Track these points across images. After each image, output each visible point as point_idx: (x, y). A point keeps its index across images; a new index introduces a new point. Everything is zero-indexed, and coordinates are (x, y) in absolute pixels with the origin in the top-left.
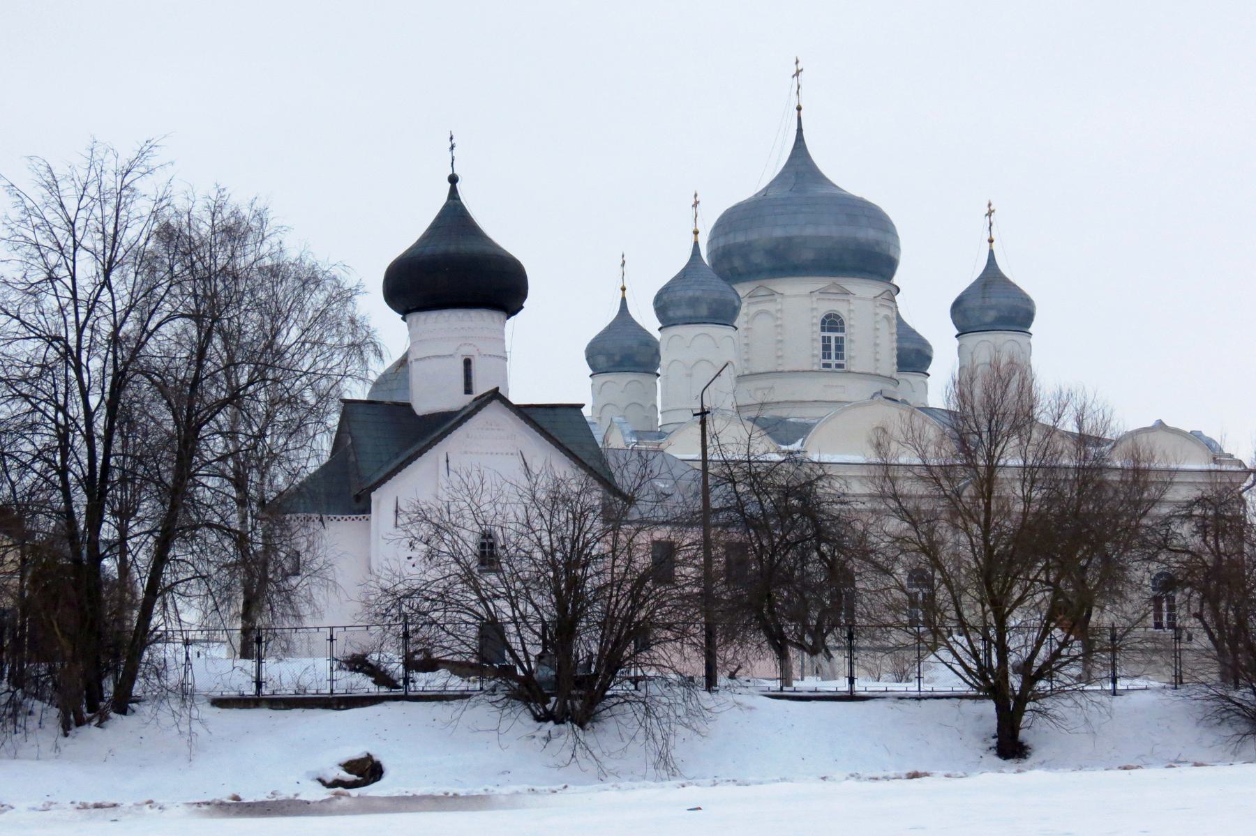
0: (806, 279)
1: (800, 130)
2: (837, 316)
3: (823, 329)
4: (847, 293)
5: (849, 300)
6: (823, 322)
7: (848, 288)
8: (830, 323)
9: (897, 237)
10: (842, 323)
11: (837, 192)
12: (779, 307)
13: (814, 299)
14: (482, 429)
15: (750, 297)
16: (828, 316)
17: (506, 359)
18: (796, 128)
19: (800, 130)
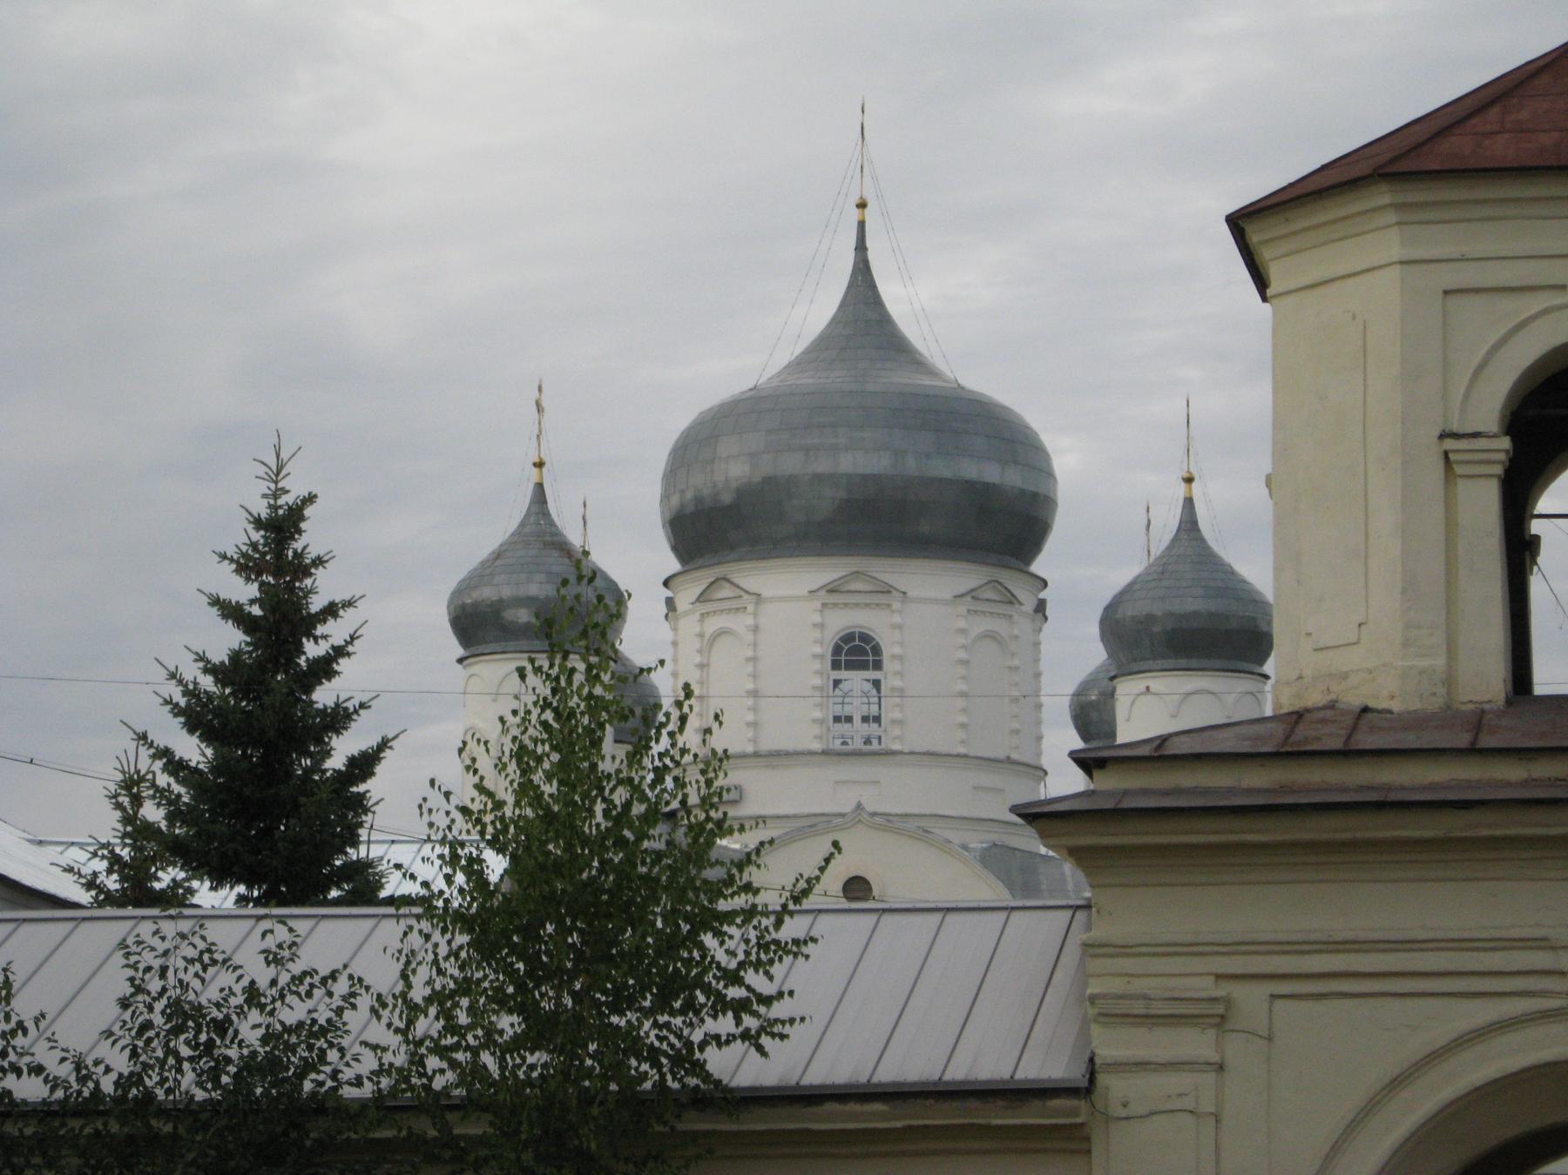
0: (950, 564)
1: (861, 247)
2: (865, 638)
3: (836, 665)
4: (887, 590)
5: (1011, 616)
6: (837, 650)
7: (887, 578)
8: (850, 652)
9: (1055, 478)
10: (877, 650)
11: (1528, 563)
12: (897, 619)
13: (962, 609)
14: (500, 759)
15: (831, 591)
16: (848, 638)
17: (1366, 710)
18: (853, 245)
19: (861, 247)
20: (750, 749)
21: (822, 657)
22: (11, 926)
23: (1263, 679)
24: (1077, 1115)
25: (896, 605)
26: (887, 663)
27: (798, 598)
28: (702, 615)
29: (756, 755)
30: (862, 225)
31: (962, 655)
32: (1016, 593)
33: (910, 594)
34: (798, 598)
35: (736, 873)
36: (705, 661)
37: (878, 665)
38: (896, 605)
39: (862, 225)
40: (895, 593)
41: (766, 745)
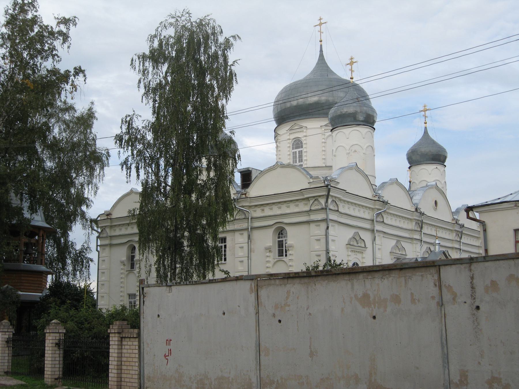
1: (321, 51)
19: (321, 51)
20: (324, 165)
21: (289, 147)
22: (368, 176)
23: (331, 168)
24: (171, 280)
25: (305, 131)
26: (304, 146)
27: (317, 128)
28: (290, 134)
29: (326, 167)
30: (321, 46)
31: (324, 141)
32: (303, 125)
33: (308, 127)
34: (317, 128)
35: (98, 170)
36: (326, 141)
37: (302, 147)
38: (305, 131)
39: (321, 46)
40: (304, 128)
41: (328, 165)
